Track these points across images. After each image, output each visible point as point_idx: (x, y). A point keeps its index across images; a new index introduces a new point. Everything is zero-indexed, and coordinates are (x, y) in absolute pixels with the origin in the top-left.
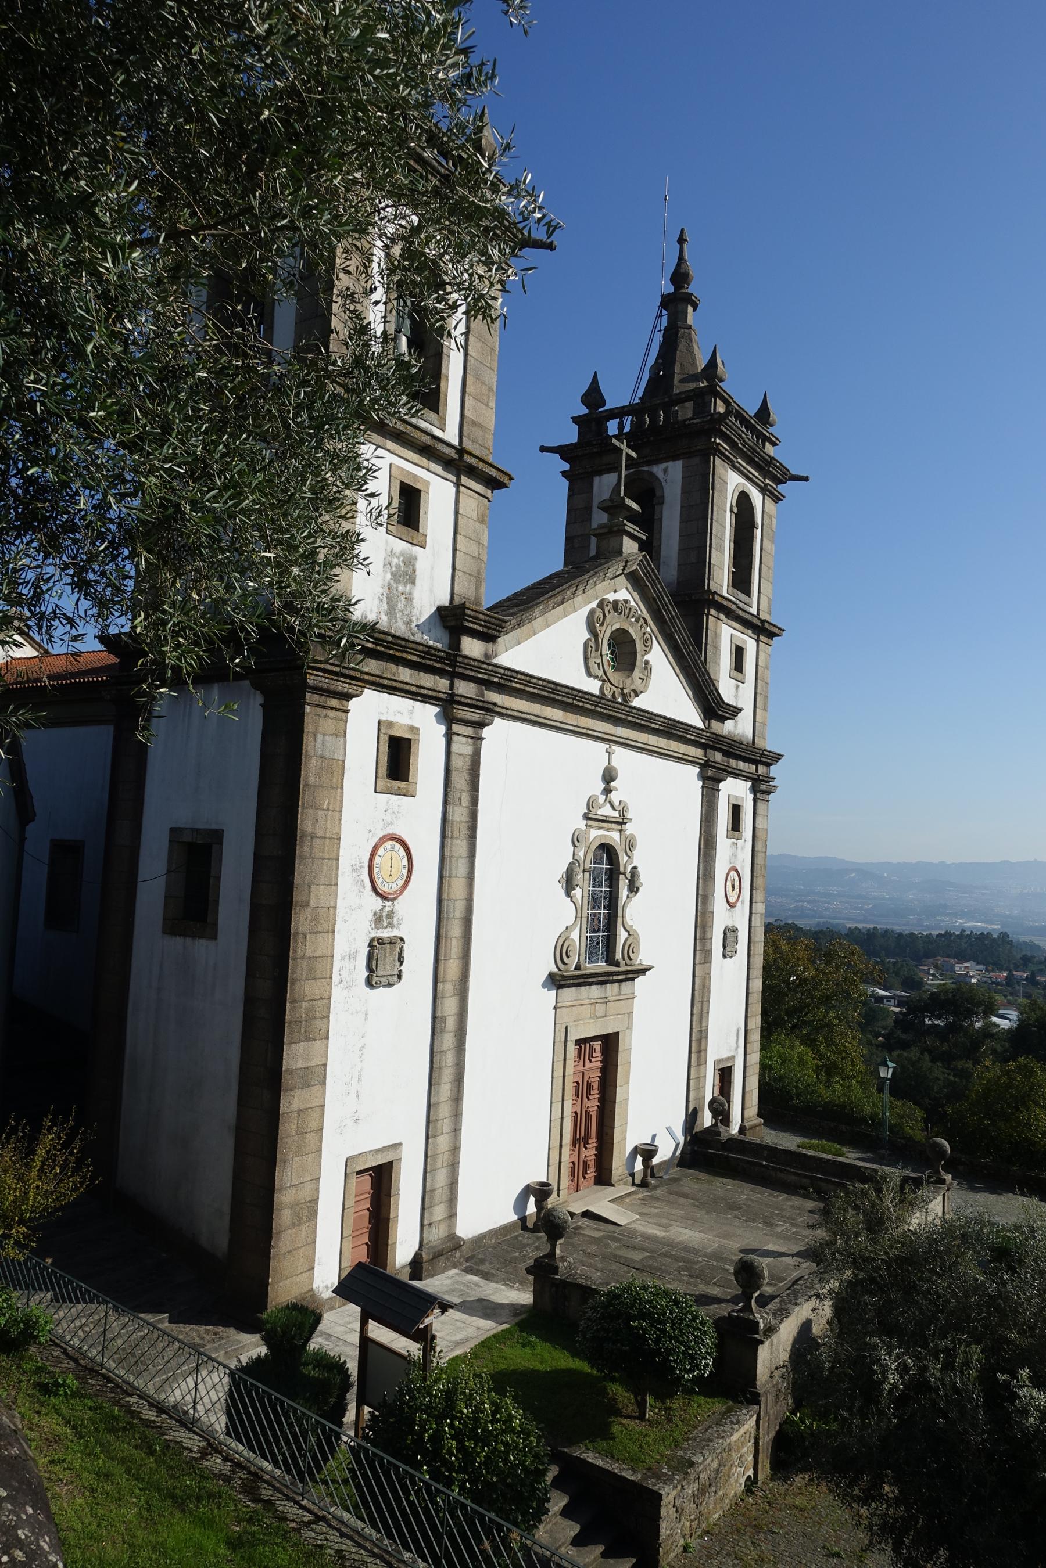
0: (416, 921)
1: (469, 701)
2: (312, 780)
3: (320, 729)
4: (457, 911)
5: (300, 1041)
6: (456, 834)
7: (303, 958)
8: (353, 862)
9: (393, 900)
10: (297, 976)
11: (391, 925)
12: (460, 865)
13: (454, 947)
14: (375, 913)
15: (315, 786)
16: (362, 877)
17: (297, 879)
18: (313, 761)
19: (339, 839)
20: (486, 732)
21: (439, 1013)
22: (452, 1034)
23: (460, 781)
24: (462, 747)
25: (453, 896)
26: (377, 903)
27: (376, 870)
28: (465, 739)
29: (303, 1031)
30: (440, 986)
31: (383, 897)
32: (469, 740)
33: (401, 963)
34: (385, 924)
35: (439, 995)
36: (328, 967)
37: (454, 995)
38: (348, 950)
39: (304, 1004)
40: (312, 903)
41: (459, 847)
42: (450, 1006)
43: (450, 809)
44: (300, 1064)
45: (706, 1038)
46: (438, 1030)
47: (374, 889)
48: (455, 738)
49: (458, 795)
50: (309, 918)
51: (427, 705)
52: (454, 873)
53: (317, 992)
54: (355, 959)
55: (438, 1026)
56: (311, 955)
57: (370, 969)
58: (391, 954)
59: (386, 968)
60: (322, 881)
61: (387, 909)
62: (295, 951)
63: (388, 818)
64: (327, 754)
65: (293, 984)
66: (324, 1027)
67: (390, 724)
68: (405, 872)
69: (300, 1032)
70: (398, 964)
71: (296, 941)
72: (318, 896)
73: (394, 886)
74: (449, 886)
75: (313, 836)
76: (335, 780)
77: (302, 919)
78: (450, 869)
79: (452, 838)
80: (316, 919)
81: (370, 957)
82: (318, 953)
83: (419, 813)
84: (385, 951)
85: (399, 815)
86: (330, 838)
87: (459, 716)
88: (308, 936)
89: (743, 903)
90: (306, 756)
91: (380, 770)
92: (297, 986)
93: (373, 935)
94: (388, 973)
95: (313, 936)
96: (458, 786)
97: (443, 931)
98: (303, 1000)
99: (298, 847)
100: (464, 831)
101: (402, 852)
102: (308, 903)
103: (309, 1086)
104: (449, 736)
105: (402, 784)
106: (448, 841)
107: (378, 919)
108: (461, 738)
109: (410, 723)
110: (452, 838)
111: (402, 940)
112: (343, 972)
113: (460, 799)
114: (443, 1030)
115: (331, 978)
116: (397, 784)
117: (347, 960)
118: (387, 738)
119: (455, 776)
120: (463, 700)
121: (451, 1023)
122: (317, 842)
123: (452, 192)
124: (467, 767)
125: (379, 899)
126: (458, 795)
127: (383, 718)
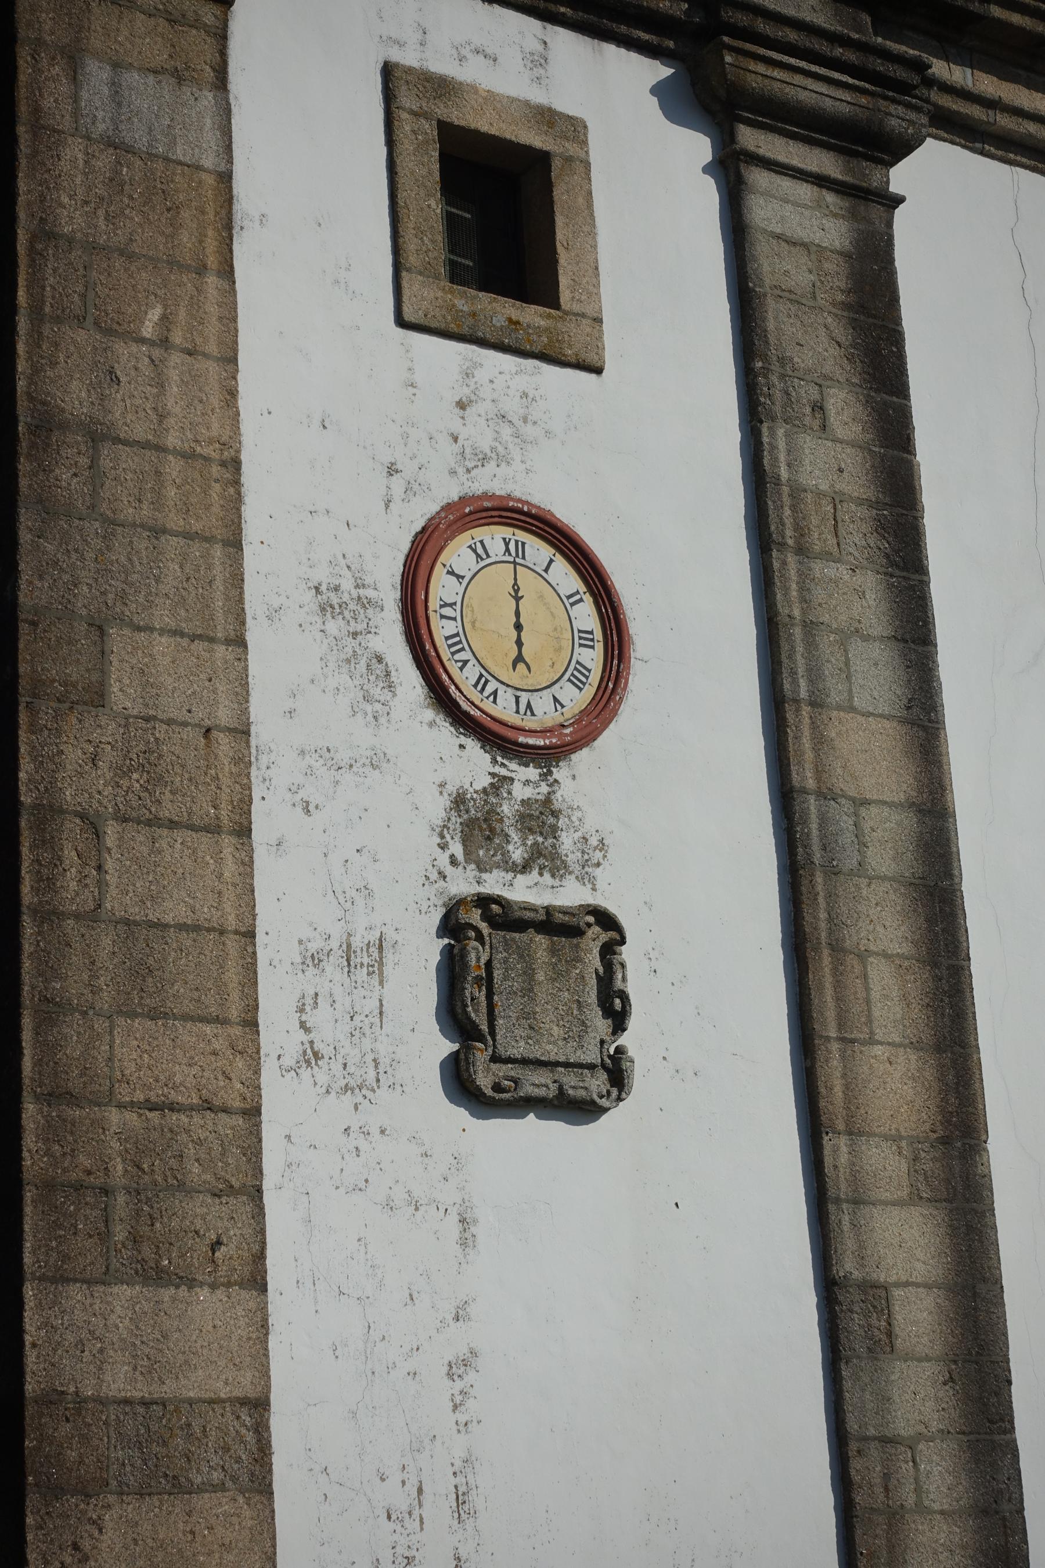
0: (676, 835)
1: (792, 36)
2: (71, 219)
3: (96, 42)
4: (883, 844)
5: (107, 1278)
6: (820, 537)
7: (93, 916)
8: (322, 575)
9: (549, 754)
10: (73, 985)
11: (545, 859)
12: (858, 666)
13: (886, 995)
14: (459, 801)
15: (93, 247)
16: (376, 644)
17: (32, 591)
18: (74, 151)
19: (235, 465)
20: (901, 177)
21: (847, 1266)
22: (929, 1371)
23: (814, 344)
24: (795, 214)
25: (839, 782)
26: (473, 766)
27: (442, 629)
28: (805, 191)
29: (120, 1233)
30: (837, 1149)
31: (495, 738)
32: (830, 198)
33: (619, 1020)
34: (517, 854)
35: (839, 1185)
36: (232, 975)
37: (915, 1198)
38: (337, 933)
39: (114, 1117)
40: (123, 694)
41: (849, 593)
42: (903, 1244)
43: (777, 437)
44: (119, 1381)
46: (855, 1340)
47: (441, 696)
48: (759, 178)
49: (807, 392)
50: (109, 755)
51: (611, 50)
52: (835, 691)
53: (182, 1074)
54: (378, 969)
55: (854, 1323)
56: (135, 913)
57: (453, 1015)
58: (557, 975)
59: (543, 1025)
60: (162, 617)
61: (520, 792)
62: (47, 883)
63: (478, 433)
64: (137, 136)
65: (47, 1020)
66: (236, 1233)
67: (441, 87)
68: (593, 658)
69: (104, 1236)
70: (602, 1025)
71: (47, 842)
72: (147, 670)
73: (543, 704)
74: (820, 741)
75: (99, 435)
76: (186, 238)
77: (73, 756)
78: (815, 675)
79: (801, 550)
80: (145, 764)
81: (452, 972)
82: (173, 911)
83: (641, 421)
84: (525, 955)
85: (351, 1415)
86: (189, 456)
87: (754, 82)
88: (111, 832)
90: (37, 128)
91: (411, 244)
92: (72, 1029)
93: (463, 883)
94: (553, 1052)
95: (140, 837)
96: (804, 359)
97: (818, 918)
98: (109, 1099)
99: (24, 466)
100: (859, 533)
101: (566, 577)
102: (97, 697)
103: (180, 1487)
104: (730, 170)
105: (531, 315)
106: (788, 566)
107: (476, 826)
108: (786, 184)
109: (538, 97)
110: (857, 1202)
111: (606, 920)
112: (320, 1017)
113: (818, 407)
114: (884, 1343)
115: (251, 1024)
116: (500, 310)
117: (333, 968)
118: (430, 129)
119: (778, 320)
120: (762, 26)
121: (919, 1318)
122: (122, 464)
123: (869, 395)
124: (837, 278)
125: (472, 745)
126: (807, 392)
127: (408, 58)
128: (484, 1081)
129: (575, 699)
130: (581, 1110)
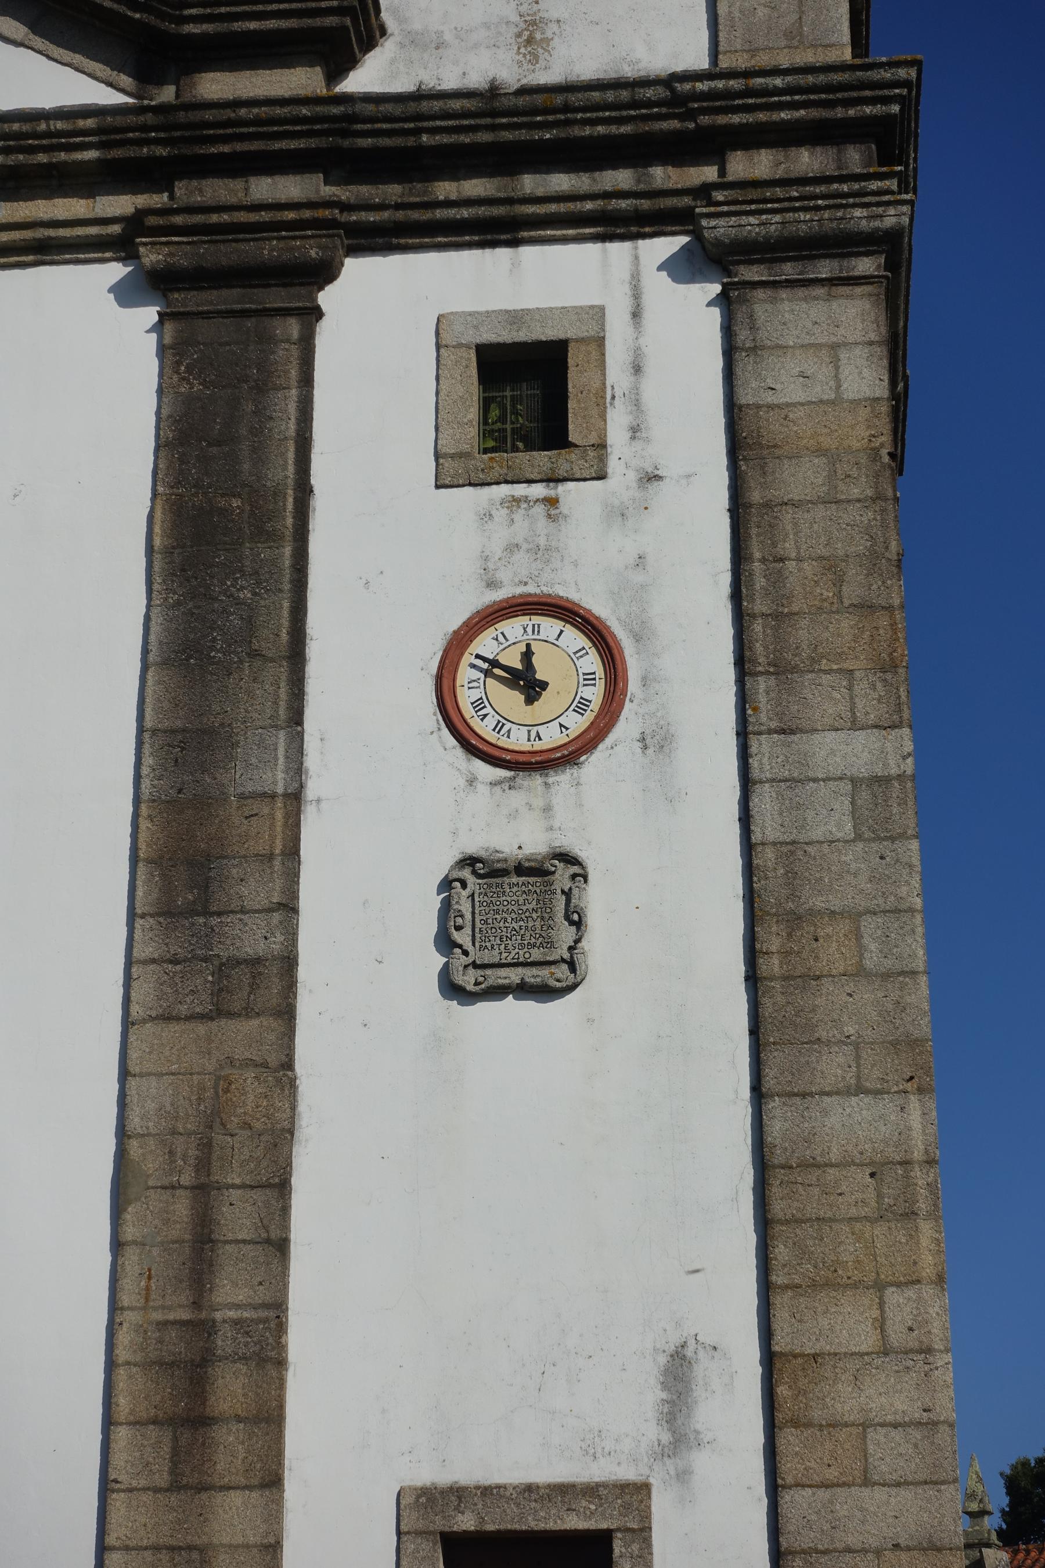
45: (268, 1356)
89: (656, 742)
128: (468, 980)
129: (577, 724)
130: (544, 992)
